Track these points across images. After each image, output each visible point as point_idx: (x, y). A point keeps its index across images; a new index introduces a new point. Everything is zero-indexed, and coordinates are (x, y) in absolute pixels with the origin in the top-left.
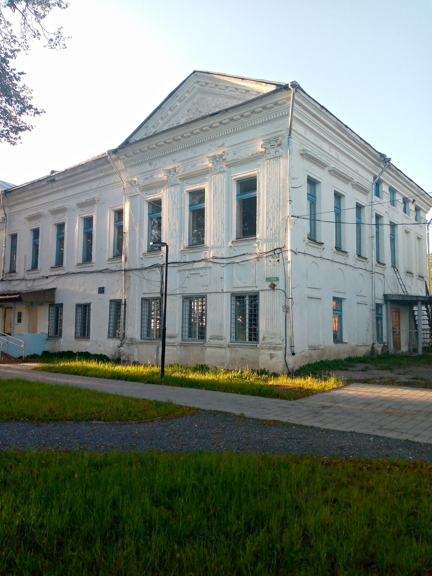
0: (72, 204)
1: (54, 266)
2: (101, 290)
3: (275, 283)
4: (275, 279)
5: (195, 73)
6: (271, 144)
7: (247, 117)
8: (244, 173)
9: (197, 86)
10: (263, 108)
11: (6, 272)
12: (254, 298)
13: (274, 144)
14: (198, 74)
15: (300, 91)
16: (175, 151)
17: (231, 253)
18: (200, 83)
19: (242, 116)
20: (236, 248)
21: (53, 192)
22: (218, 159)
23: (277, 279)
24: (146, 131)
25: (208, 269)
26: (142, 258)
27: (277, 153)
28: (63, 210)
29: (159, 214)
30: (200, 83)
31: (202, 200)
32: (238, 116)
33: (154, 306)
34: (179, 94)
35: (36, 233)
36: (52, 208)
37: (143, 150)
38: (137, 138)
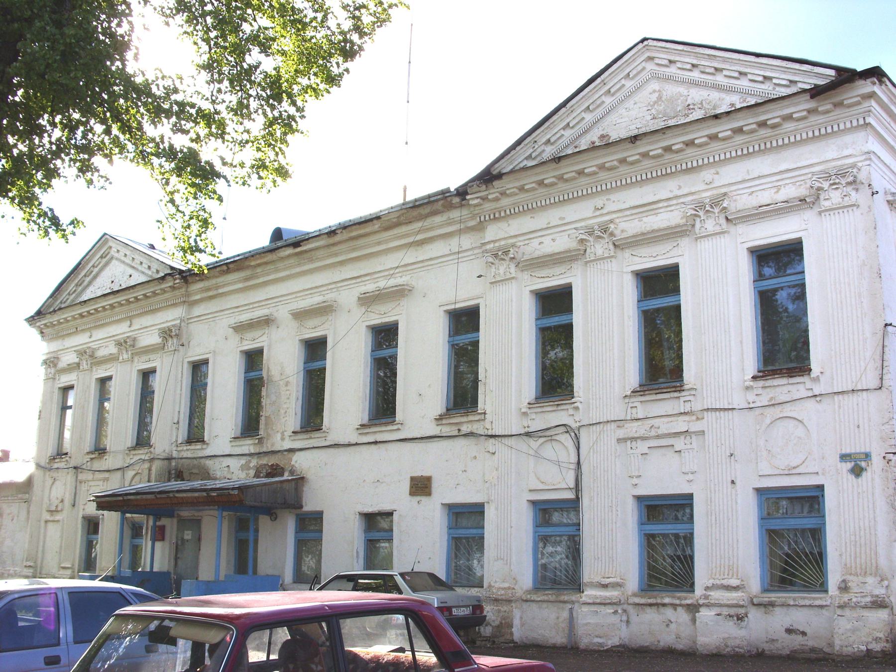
0: (282, 313)
1: (298, 429)
2: (421, 486)
3: (863, 464)
4: (863, 456)
5: (646, 43)
6: (832, 182)
7: (677, 152)
8: (653, 258)
9: (650, 66)
10: (600, 169)
11: (180, 442)
12: (811, 499)
13: (837, 181)
14: (651, 42)
15: (888, 83)
16: (693, 168)
17: (751, 401)
18: (657, 61)
19: (541, 183)
20: (534, 416)
21: (320, 267)
22: (708, 208)
23: (867, 456)
24: (532, 150)
25: (694, 437)
26: (525, 414)
27: (846, 199)
28: (325, 310)
29: (474, 335)
30: (657, 61)
31: (567, 308)
32: (615, 163)
33: (557, 519)
34: (612, 80)
35: (385, 336)
36: (364, 289)
37: (565, 177)
38: (519, 159)
